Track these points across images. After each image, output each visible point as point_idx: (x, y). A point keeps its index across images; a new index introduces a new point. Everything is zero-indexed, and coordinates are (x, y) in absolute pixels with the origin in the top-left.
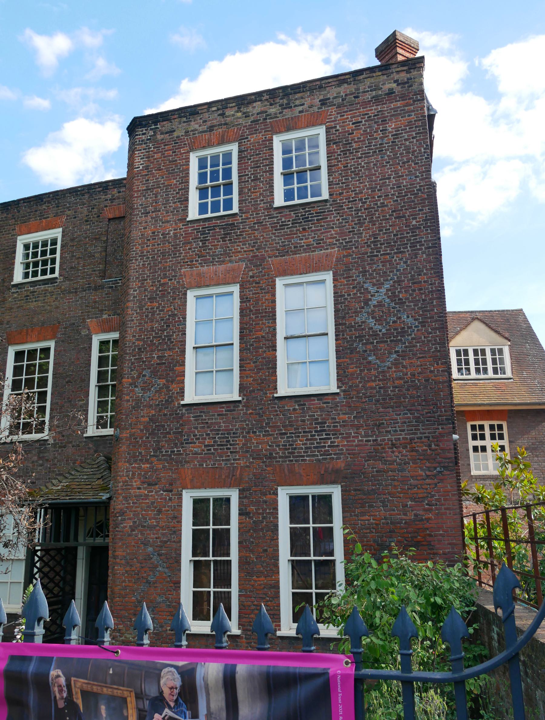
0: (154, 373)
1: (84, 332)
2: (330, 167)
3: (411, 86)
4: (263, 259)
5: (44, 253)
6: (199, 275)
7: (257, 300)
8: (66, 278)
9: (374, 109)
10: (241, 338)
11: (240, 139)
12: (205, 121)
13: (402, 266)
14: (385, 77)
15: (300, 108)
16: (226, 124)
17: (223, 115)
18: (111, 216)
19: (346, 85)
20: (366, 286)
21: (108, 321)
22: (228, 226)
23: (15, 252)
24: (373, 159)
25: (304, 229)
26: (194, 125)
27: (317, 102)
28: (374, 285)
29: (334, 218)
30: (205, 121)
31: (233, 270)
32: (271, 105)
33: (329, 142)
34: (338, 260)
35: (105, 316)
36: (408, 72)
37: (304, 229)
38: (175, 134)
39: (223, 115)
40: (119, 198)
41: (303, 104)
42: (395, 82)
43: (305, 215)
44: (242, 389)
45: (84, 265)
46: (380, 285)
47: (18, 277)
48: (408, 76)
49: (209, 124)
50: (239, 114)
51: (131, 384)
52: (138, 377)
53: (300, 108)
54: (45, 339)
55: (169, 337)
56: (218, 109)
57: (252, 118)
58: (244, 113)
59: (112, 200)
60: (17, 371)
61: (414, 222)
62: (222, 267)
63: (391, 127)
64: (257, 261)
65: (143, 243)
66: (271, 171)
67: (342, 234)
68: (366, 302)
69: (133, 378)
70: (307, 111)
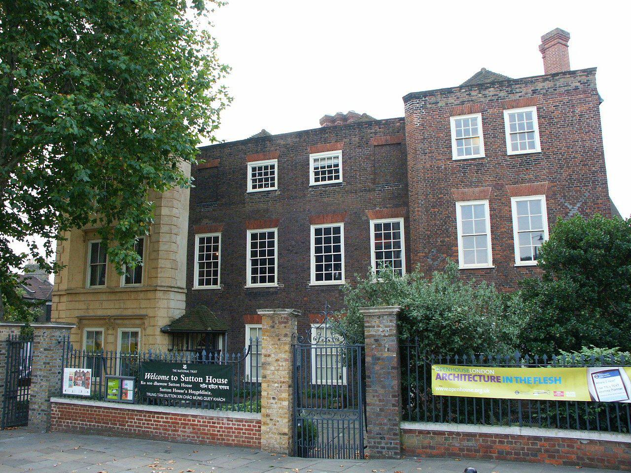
0: (439, 251)
1: (364, 218)
2: (540, 132)
3: (589, 85)
4: (502, 186)
5: (266, 174)
6: (463, 193)
7: (500, 210)
8: (348, 183)
9: (566, 99)
10: (492, 232)
11: (483, 112)
12: (458, 98)
13: (587, 194)
14: (573, 79)
15: (520, 94)
16: (472, 101)
17: (469, 94)
18: (376, 144)
19: (548, 82)
20: (566, 204)
21: (380, 212)
22: (477, 164)
23: (309, 164)
24: (567, 129)
25: (527, 169)
26: (451, 100)
27: (530, 91)
28: (570, 204)
29: (544, 163)
30: (458, 98)
31: (484, 191)
32: (500, 90)
33: (539, 117)
34: (549, 189)
35: (378, 209)
36: (587, 76)
37: (527, 169)
38: (439, 105)
39: (469, 94)
40: (380, 132)
41: (521, 92)
42: (579, 82)
43: (525, 160)
44: (494, 262)
45: (360, 175)
46: (574, 204)
47: (312, 182)
48: (587, 78)
49: (461, 100)
50: (480, 95)
51: (425, 257)
52: (429, 253)
53: (520, 94)
54: (337, 222)
55: (447, 230)
56: (466, 91)
57: (489, 98)
58: (483, 95)
59: (375, 133)
60: (318, 241)
61: (594, 169)
62: (477, 189)
63: (578, 110)
64: (498, 187)
65: (425, 172)
66: (504, 132)
67: (550, 173)
68: (567, 214)
69: (426, 253)
70: (524, 96)
